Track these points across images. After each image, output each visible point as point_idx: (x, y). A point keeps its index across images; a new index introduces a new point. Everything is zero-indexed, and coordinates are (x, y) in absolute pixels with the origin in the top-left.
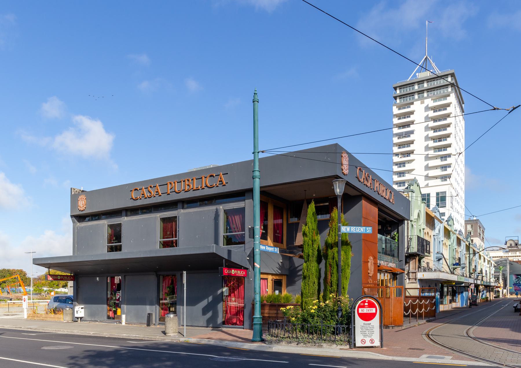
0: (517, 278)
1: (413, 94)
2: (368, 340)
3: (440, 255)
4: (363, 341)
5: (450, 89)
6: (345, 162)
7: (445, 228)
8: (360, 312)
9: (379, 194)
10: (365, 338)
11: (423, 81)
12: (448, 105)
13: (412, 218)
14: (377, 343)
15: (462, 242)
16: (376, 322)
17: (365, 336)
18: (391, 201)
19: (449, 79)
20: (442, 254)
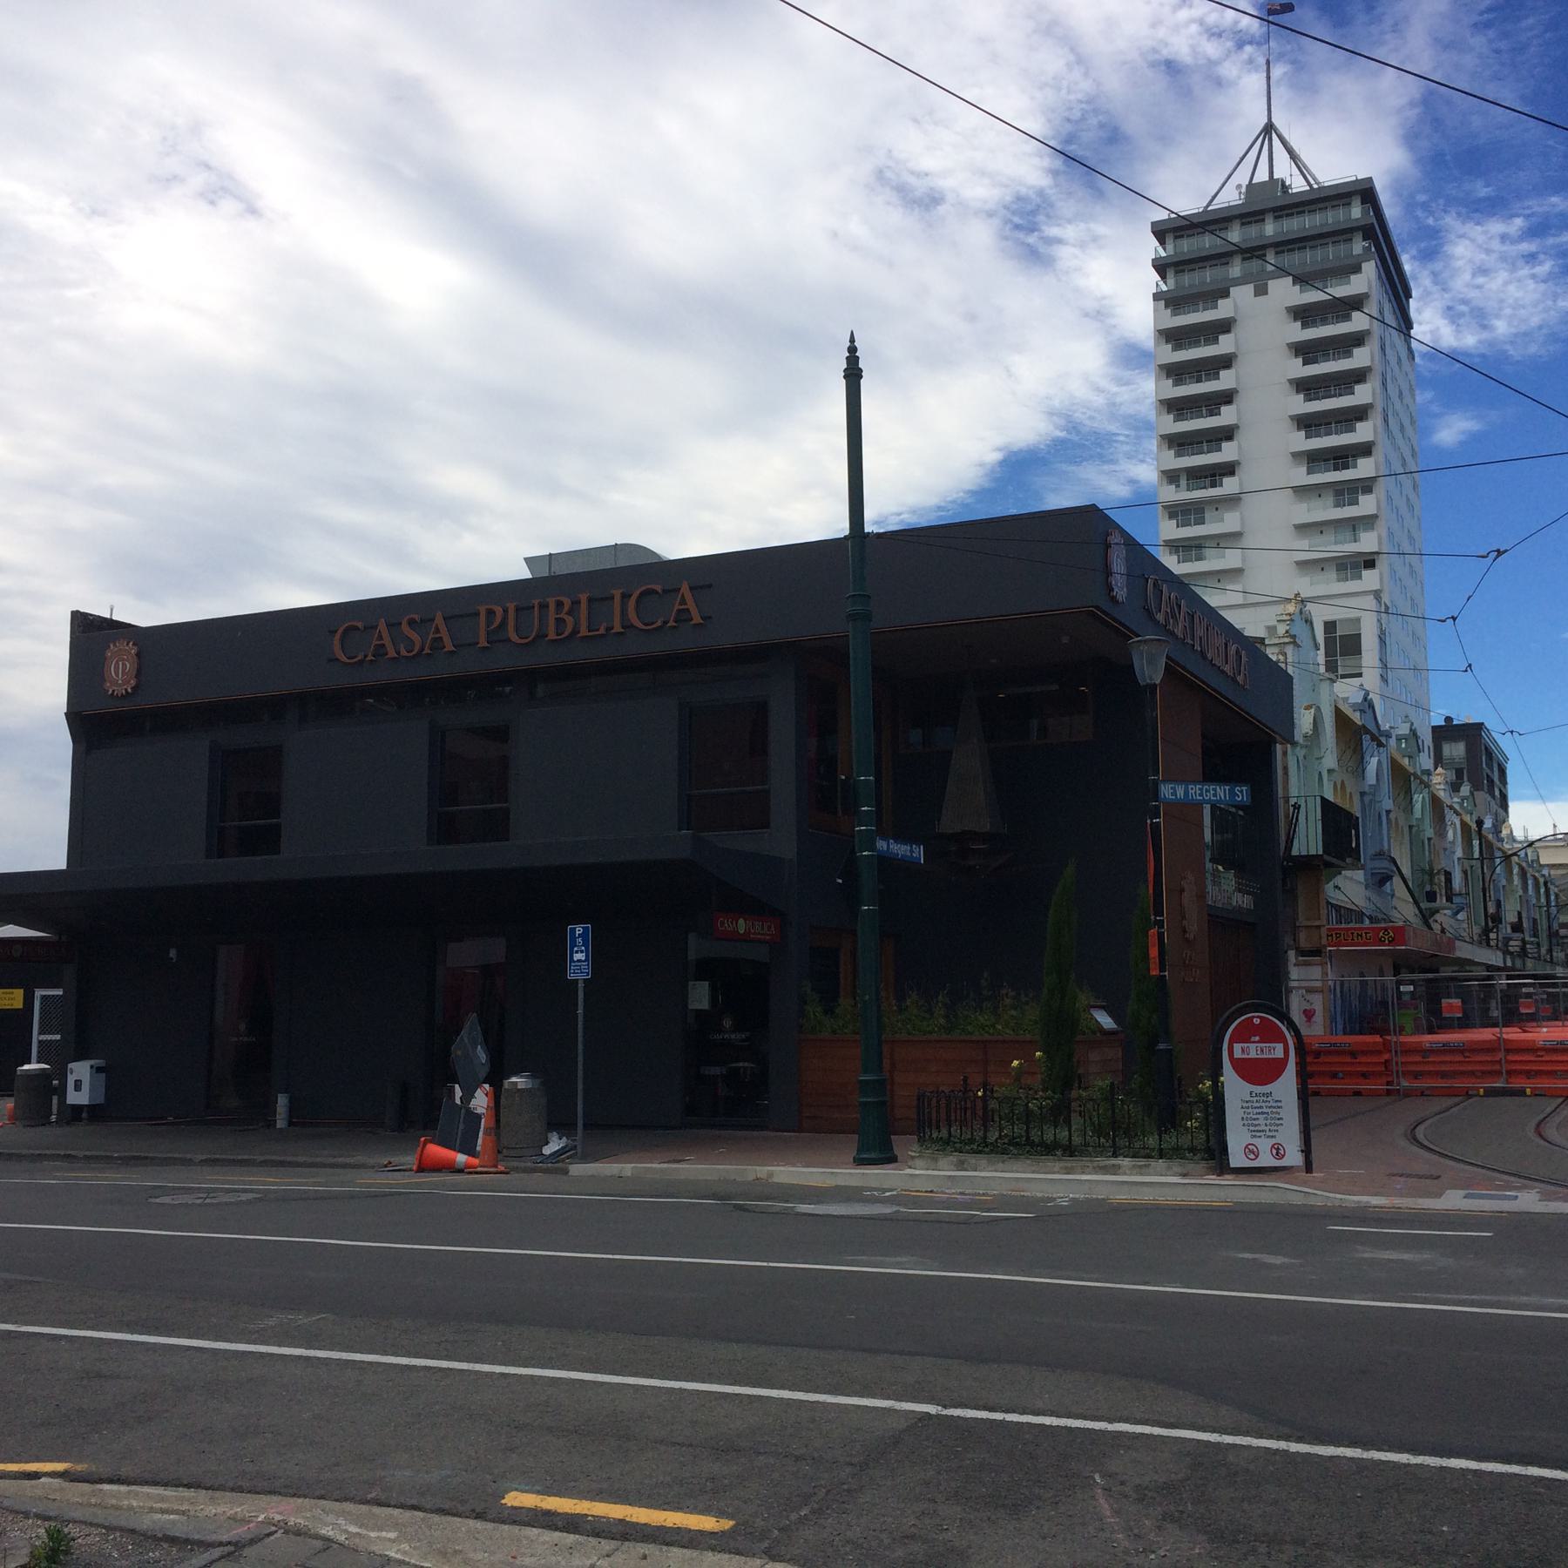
2: (1264, 1145)
3: (1385, 864)
4: (1251, 1151)
5: (1359, 246)
6: (1118, 564)
7: (1396, 767)
8: (1238, 1054)
9: (1204, 657)
10: (1254, 1141)
11: (1262, 212)
13: (1298, 737)
14: (1294, 1157)
15: (1450, 817)
16: (1286, 1087)
17: (1256, 1133)
18: (1240, 679)
19: (1356, 211)
20: (1394, 861)
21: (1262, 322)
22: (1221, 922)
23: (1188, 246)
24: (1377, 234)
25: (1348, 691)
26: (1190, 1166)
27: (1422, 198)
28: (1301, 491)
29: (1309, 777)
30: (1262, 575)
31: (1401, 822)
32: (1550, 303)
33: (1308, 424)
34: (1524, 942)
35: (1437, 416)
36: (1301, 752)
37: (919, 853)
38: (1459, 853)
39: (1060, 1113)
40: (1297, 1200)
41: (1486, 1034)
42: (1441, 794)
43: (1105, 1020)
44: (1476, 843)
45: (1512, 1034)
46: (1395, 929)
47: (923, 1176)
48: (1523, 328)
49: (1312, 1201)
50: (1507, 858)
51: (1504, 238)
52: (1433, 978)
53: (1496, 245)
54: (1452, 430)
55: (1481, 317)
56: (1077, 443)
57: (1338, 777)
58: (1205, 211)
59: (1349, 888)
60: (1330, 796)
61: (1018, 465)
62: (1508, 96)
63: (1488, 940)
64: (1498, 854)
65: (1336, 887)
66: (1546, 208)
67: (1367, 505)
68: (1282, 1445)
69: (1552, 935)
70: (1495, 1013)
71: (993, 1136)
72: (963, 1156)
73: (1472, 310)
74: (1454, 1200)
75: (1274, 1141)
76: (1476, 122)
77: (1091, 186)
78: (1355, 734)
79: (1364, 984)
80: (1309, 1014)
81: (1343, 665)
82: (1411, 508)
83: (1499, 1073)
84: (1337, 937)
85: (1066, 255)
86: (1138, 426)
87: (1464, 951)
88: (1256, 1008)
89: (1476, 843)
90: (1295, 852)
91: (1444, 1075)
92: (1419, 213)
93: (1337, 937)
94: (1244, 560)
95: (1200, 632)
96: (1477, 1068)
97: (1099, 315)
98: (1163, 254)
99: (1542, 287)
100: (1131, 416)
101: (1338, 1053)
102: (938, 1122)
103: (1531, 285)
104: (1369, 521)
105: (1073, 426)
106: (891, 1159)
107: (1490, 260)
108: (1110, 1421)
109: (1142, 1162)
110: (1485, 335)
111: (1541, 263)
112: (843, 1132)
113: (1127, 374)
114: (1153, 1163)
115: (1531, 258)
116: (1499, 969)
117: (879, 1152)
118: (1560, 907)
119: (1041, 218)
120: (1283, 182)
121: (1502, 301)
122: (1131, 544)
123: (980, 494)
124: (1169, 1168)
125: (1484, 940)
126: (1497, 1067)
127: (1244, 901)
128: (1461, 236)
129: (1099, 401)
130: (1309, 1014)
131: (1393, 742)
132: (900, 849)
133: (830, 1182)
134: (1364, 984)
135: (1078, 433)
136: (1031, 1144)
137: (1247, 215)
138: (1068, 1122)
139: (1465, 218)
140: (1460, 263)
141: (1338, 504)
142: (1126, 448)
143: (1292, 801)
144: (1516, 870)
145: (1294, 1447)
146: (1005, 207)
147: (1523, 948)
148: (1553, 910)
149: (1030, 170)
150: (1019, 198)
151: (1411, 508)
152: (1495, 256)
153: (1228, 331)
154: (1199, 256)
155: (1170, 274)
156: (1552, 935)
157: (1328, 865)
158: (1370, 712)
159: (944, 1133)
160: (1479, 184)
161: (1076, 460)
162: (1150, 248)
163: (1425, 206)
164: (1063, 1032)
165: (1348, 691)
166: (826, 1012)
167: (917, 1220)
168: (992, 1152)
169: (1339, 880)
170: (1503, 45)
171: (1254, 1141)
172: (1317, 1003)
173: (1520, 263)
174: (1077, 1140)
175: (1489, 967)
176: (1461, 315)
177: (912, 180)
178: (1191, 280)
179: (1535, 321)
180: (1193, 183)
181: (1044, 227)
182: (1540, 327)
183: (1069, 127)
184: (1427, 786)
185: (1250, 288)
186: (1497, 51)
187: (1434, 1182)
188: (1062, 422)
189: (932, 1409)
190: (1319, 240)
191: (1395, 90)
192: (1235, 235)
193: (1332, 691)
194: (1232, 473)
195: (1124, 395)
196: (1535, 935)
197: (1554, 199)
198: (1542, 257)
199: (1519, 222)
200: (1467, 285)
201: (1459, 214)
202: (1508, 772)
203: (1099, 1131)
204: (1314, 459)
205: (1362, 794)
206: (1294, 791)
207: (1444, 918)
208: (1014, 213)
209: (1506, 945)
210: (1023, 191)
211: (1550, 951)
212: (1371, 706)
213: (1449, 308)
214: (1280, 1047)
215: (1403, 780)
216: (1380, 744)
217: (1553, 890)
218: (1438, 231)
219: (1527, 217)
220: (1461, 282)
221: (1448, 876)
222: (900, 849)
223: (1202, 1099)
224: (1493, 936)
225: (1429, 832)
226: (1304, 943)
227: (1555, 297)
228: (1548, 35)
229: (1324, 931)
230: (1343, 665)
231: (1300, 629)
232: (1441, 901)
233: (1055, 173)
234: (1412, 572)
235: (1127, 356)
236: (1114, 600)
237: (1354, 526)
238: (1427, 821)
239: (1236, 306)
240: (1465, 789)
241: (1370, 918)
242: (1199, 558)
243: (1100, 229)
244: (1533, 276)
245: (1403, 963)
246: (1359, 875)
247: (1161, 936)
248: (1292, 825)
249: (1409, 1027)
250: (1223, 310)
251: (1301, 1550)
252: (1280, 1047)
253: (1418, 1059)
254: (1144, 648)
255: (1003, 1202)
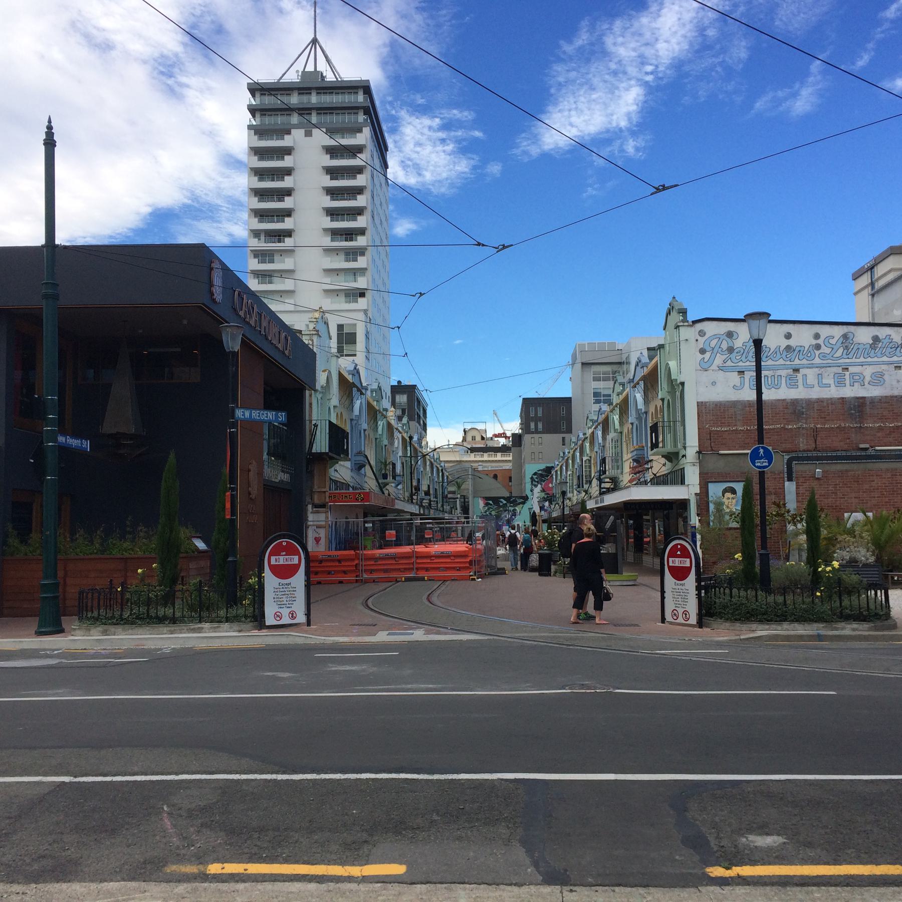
0: (487, 504)
1: (288, 110)
2: (285, 612)
3: (362, 458)
4: (278, 616)
5: (361, 117)
6: (217, 280)
8: (273, 562)
9: (267, 339)
10: (280, 610)
11: (310, 89)
12: (359, 149)
13: (318, 387)
14: (301, 618)
15: (396, 434)
16: (299, 580)
17: (281, 606)
18: (287, 352)
19: (361, 98)
21: (309, 150)
22: (270, 488)
23: (269, 101)
24: (370, 111)
25: (345, 363)
26: (243, 626)
27: (390, 99)
28: (328, 251)
29: (323, 409)
30: (304, 296)
31: (372, 436)
32: (452, 166)
33: (332, 213)
34: (430, 501)
35: (396, 219)
36: (319, 396)
37: (86, 445)
38: (400, 454)
39: (168, 599)
40: (300, 641)
41: (407, 549)
42: (393, 422)
43: (200, 545)
44: (409, 448)
45: (420, 549)
46: (365, 494)
47: (81, 640)
48: (439, 178)
49: (308, 642)
50: (424, 456)
51: (430, 128)
52: (383, 520)
53: (426, 131)
54: (403, 228)
55: (418, 169)
56: (197, 209)
57: (339, 410)
58: (278, 82)
59: (342, 471)
60: (334, 421)
61: (161, 217)
62: (432, 49)
63: (412, 499)
64: (420, 454)
65: (336, 470)
66: (451, 116)
67: (362, 262)
68: (274, 776)
69: (444, 497)
70: (413, 538)
71: (126, 614)
72: (105, 627)
73: (414, 165)
74: (383, 637)
75: (290, 610)
76: (417, 62)
77: (206, 56)
78: (349, 387)
79: (347, 523)
80: (317, 540)
81: (347, 349)
82: (384, 266)
83: (413, 569)
84: (333, 497)
85: (191, 95)
86: (236, 204)
87: (399, 505)
88: (284, 537)
89: (409, 448)
90: (314, 451)
91: (386, 571)
92: (388, 107)
93: (333, 497)
94: (295, 286)
95: (264, 324)
96: (401, 567)
97: (211, 134)
98: (254, 103)
99: (448, 157)
100: (230, 197)
101: (333, 561)
102: (92, 607)
103: (443, 155)
104: (362, 271)
105: (195, 198)
106: (60, 631)
107: (423, 139)
108: (177, 774)
109: (216, 625)
110: (420, 179)
111: (448, 145)
112: (31, 616)
113: (228, 172)
114: (222, 625)
115: (443, 141)
116: (416, 515)
117: (52, 625)
118: (449, 483)
119: (176, 70)
120: (322, 74)
121: (429, 162)
122: (225, 269)
123: (137, 231)
124: (231, 628)
125: (411, 500)
126: (411, 566)
127: (285, 477)
128: (409, 123)
129: (211, 185)
130: (317, 540)
131: (369, 393)
132: (74, 442)
133: (18, 647)
134: (347, 523)
135: (198, 202)
136: (151, 618)
137: (303, 89)
138: (173, 604)
139: (411, 114)
140: (408, 138)
141: (347, 260)
142: (227, 215)
143: (314, 422)
144: (428, 463)
145: (280, 777)
146: (155, 60)
147: (430, 504)
148: (445, 484)
149: (172, 42)
150: (162, 56)
151: (384, 266)
152: (425, 137)
153: (290, 154)
154: (275, 107)
155: (258, 115)
156: (444, 497)
157: (332, 458)
158: (357, 375)
159: (95, 614)
160: (418, 96)
161: (195, 218)
162: (247, 98)
163: (391, 103)
164: (171, 553)
165: (345, 363)
166: (22, 542)
167: (71, 667)
168: (125, 624)
169: (337, 467)
170: (429, 21)
171: (280, 610)
172: (322, 533)
173: (438, 143)
174: (178, 614)
175: (412, 514)
176: (409, 166)
177: (94, 32)
178: (269, 120)
179: (445, 175)
180: (277, 64)
181: (178, 76)
182: (447, 179)
183: (193, 19)
184: (385, 417)
185: (302, 131)
186: (428, 25)
187: (373, 627)
188: (189, 194)
189: (66, 779)
190: (338, 109)
191: (376, 36)
192: (294, 99)
193: (337, 361)
194: (290, 236)
195: (458, 168)
196: (436, 497)
197: (455, 112)
198: (448, 142)
199: (437, 121)
200: (411, 151)
201: (408, 111)
202: (428, 412)
203: (191, 608)
204: (335, 233)
205: (352, 420)
206: (314, 417)
207: (391, 488)
208: (160, 64)
209: (421, 503)
210: (165, 52)
211: (443, 506)
212: (358, 372)
213: (402, 162)
214: (296, 558)
215: (373, 413)
216: (362, 394)
217: (446, 474)
218: (398, 119)
219: (441, 119)
220: (409, 148)
221: (394, 465)
222: (74, 442)
223: (251, 587)
224: (415, 497)
225: (385, 442)
226: (316, 501)
227: (454, 163)
228: (453, 22)
229: (327, 494)
230: (347, 349)
231: (321, 327)
232: (390, 479)
233: (185, 45)
234: (384, 302)
235: (230, 162)
236: (214, 301)
237: (356, 273)
238: (385, 436)
239: (294, 140)
240: (405, 420)
241: (353, 488)
242: (270, 282)
243: (212, 84)
244: (444, 151)
245: (368, 512)
246: (348, 464)
247: (233, 498)
248: (313, 435)
249: (369, 544)
250: (287, 141)
251: (276, 833)
252: (296, 558)
253: (372, 563)
254: (229, 330)
255: (129, 653)
